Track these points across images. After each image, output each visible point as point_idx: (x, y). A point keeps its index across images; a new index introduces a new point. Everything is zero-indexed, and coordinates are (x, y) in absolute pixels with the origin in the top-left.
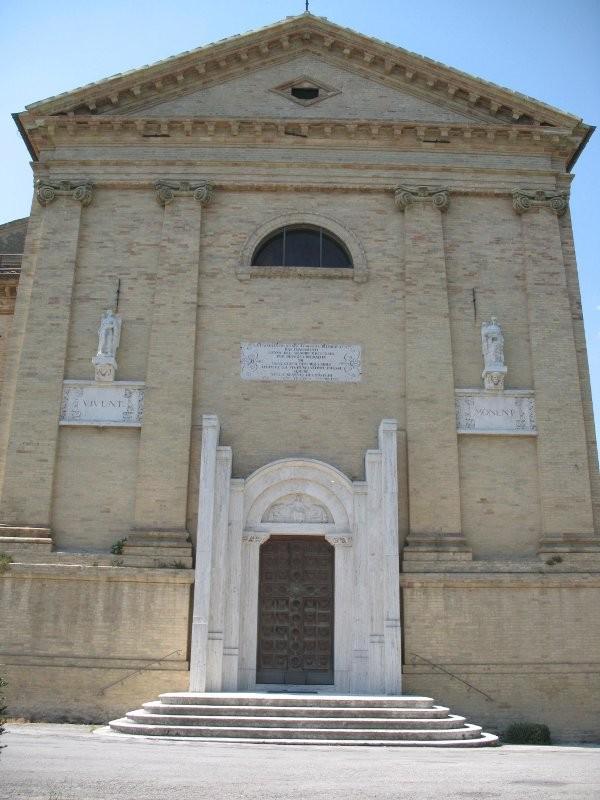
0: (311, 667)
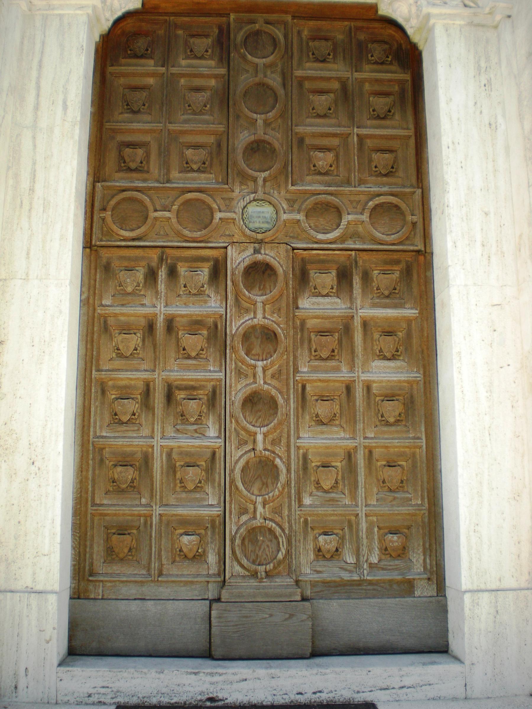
0: (331, 572)
